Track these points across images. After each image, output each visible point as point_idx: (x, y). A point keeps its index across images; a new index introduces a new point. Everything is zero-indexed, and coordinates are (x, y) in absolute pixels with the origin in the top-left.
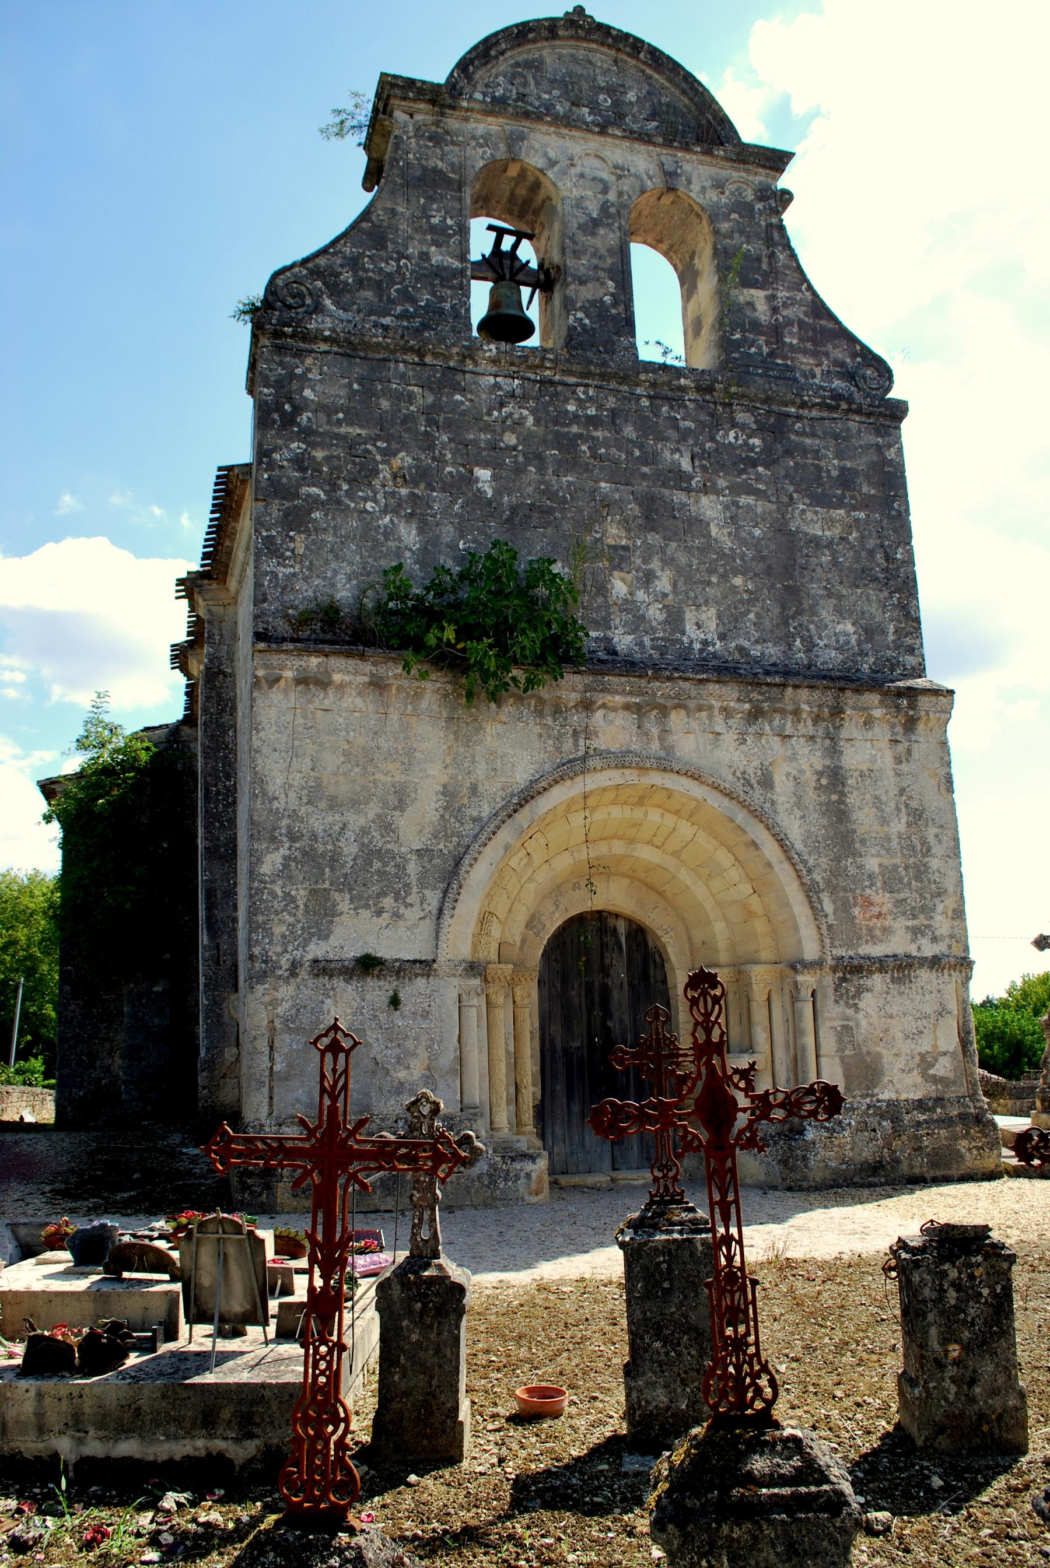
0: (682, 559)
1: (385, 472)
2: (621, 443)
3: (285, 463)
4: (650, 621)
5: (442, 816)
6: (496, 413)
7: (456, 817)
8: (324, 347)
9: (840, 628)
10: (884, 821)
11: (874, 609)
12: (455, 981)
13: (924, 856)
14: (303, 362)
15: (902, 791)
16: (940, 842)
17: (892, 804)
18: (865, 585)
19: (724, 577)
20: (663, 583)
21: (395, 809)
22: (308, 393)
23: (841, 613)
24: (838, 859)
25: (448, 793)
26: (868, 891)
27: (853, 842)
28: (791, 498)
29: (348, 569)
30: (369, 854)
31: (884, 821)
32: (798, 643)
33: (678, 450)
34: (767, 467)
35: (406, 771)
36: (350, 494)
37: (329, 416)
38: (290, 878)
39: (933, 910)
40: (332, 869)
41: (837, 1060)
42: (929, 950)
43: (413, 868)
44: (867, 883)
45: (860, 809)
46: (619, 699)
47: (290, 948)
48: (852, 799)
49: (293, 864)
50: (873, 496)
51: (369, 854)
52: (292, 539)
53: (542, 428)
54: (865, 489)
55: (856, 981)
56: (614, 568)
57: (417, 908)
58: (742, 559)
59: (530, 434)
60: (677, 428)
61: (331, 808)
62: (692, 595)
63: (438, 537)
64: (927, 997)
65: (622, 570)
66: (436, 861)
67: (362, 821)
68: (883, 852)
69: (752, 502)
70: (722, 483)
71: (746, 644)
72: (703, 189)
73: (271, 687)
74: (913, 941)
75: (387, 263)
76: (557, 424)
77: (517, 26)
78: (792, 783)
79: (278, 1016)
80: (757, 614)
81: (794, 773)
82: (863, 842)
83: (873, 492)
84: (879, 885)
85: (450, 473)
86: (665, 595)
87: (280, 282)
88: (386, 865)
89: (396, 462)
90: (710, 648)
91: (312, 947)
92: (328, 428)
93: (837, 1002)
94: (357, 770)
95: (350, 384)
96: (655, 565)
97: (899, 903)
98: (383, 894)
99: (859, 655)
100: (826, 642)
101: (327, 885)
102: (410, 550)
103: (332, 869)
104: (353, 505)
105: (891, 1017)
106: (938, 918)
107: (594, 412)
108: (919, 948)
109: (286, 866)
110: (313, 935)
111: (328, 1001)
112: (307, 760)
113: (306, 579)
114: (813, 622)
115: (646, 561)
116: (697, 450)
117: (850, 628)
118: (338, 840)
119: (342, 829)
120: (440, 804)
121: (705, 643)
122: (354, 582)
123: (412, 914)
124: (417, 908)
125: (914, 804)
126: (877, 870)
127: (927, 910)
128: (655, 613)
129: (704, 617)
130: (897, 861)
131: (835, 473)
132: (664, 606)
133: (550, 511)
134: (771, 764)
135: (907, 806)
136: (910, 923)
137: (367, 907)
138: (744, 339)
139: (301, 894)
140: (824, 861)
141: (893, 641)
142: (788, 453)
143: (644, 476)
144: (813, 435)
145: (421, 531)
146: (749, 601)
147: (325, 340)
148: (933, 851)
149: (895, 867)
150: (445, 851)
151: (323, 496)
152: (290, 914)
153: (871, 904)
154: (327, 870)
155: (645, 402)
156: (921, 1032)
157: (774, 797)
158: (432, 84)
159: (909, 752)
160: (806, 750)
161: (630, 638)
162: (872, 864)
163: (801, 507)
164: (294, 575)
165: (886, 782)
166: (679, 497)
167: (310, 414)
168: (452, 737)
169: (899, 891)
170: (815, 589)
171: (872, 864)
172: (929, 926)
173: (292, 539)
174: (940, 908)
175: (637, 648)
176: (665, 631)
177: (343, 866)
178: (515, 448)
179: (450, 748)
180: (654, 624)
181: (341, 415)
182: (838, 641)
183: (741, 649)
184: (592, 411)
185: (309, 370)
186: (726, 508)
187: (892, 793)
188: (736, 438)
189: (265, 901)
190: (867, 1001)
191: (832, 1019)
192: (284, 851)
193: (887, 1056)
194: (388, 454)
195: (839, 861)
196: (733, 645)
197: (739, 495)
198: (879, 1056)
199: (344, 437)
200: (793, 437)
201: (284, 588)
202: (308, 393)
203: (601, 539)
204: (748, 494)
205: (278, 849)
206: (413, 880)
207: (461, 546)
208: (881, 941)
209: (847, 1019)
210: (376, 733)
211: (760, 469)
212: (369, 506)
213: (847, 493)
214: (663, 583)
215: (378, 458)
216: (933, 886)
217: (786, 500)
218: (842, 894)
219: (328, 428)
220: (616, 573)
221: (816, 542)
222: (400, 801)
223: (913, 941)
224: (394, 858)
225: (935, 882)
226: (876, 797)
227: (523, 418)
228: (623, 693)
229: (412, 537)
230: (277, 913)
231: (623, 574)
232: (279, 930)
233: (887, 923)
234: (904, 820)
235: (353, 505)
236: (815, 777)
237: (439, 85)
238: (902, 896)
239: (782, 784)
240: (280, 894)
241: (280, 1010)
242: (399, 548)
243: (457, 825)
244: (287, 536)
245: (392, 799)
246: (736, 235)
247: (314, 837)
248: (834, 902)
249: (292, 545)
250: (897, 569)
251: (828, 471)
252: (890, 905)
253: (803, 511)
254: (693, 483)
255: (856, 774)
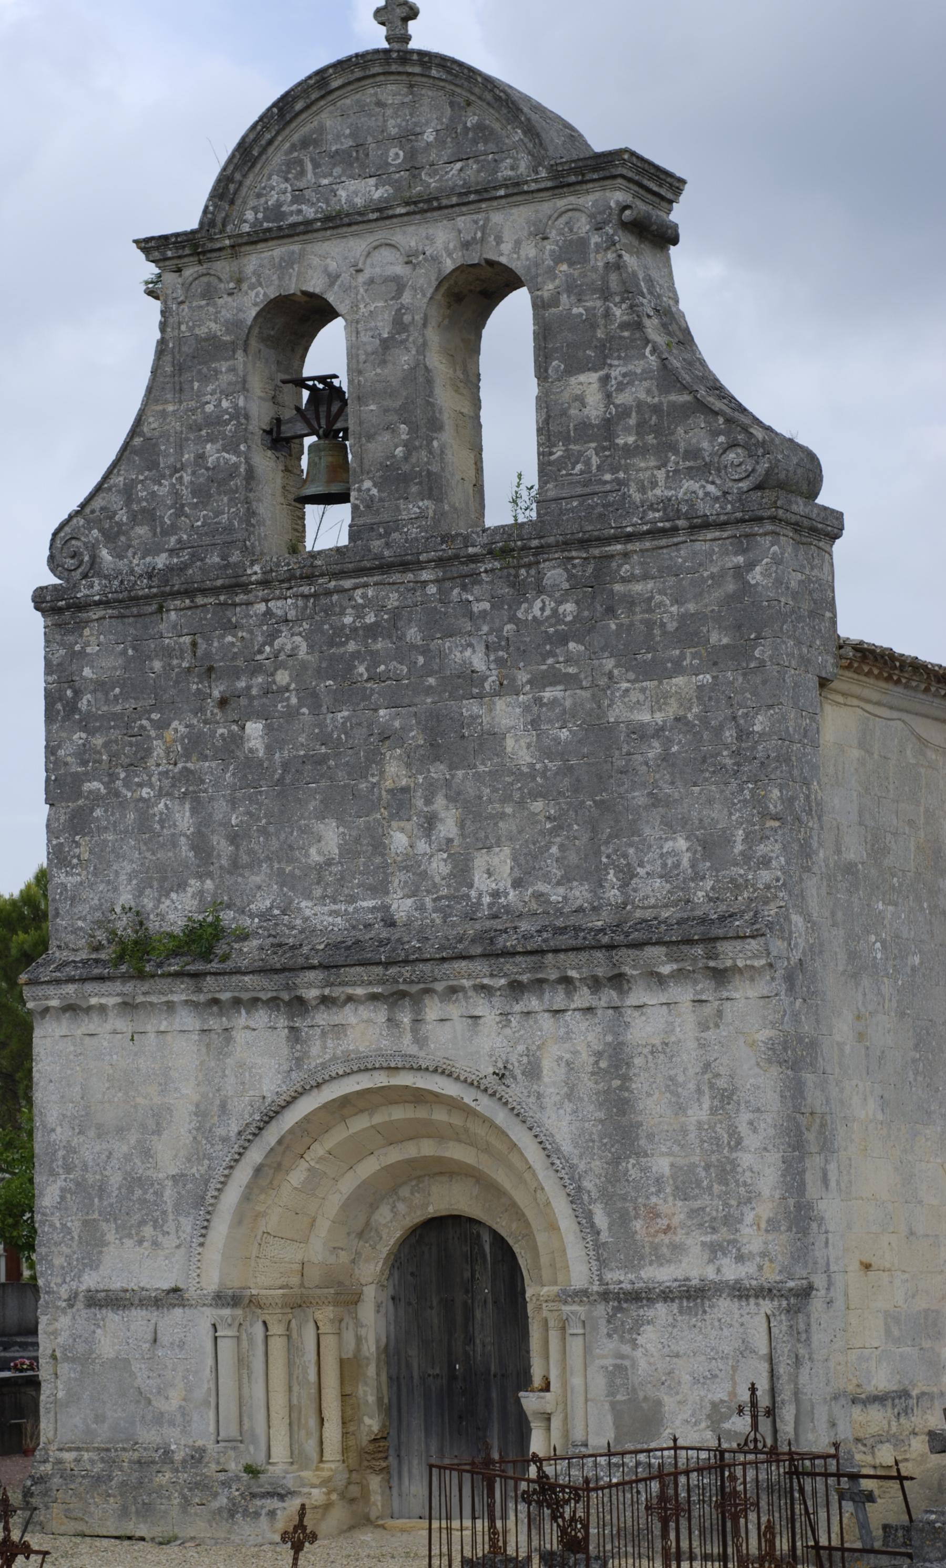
0: (470, 790)
1: (159, 748)
2: (403, 652)
3: (69, 759)
4: (432, 878)
5: (195, 1138)
6: (267, 649)
7: (207, 1138)
8: (100, 613)
9: (668, 846)
10: (680, 1108)
11: (717, 813)
12: (208, 1311)
13: (732, 1149)
14: (81, 636)
15: (707, 1066)
16: (755, 1130)
17: (692, 1086)
18: (706, 780)
19: (521, 803)
20: (448, 827)
21: (153, 1133)
22: (87, 672)
23: (670, 827)
24: (616, 1161)
25: (200, 1113)
26: (654, 1199)
27: (637, 1138)
28: (610, 675)
29: (129, 868)
30: (134, 1182)
31: (680, 1108)
32: (611, 876)
33: (470, 645)
34: (579, 641)
35: (163, 1092)
36: (127, 784)
37: (106, 694)
38: (66, 1209)
39: (740, 1221)
40: (101, 1199)
41: (607, 1406)
42: (732, 1271)
43: (169, 1194)
44: (653, 1189)
45: (649, 1095)
46: (360, 991)
47: (68, 1279)
48: (639, 1085)
49: (69, 1196)
50: (726, 647)
51: (134, 1182)
52: (78, 845)
53: (317, 655)
54: (714, 638)
55: (634, 1311)
56: (392, 817)
57: (173, 1236)
58: (544, 774)
59: (304, 665)
60: (471, 615)
61: (99, 1136)
62: (482, 834)
63: (211, 815)
64: (726, 1332)
65: (401, 819)
66: (190, 1186)
67: (125, 1149)
68: (676, 1149)
69: (559, 695)
70: (522, 677)
71: (542, 887)
72: (518, 243)
73: (43, 1018)
74: (711, 1261)
75: (160, 484)
76: (331, 644)
77: (275, 105)
78: (563, 1070)
79: (58, 1344)
80: (562, 847)
81: (567, 1056)
82: (650, 1137)
83: (725, 641)
84: (668, 1190)
85: (222, 735)
86: (449, 841)
87: (58, 543)
88: (145, 1192)
89: (169, 734)
90: (502, 900)
91: (86, 1277)
92: (105, 708)
93: (609, 1336)
94: (120, 1094)
95: (124, 652)
96: (440, 802)
97: (693, 1213)
98: (142, 1223)
99: (692, 880)
100: (648, 868)
101: (96, 1216)
102: (185, 835)
103: (101, 1199)
104: (129, 794)
105: (677, 1356)
106: (746, 1230)
107: (373, 620)
108: (719, 1270)
109: (63, 1198)
110: (85, 1265)
111: (99, 1331)
112: (78, 1088)
113: (91, 886)
114: (631, 845)
115: (428, 802)
116: (492, 638)
117: (682, 844)
118: (105, 1169)
119: (109, 1157)
120: (193, 1125)
121: (495, 894)
122: (134, 882)
123: (169, 1242)
124: (173, 1236)
125: (721, 1083)
126: (667, 1171)
127: (731, 1221)
128: (439, 867)
129: (496, 861)
130: (696, 1159)
131: (671, 626)
132: (450, 856)
133: (323, 759)
134: (539, 1048)
135: (712, 1086)
136: (708, 1239)
137: (130, 1236)
138: (568, 454)
139: (75, 1226)
140: (597, 1164)
141: (742, 853)
142: (610, 611)
143: (429, 690)
144: (645, 577)
145: (194, 811)
146: (551, 832)
147: (98, 604)
148: (746, 1143)
149: (692, 1167)
150: (197, 1176)
151: (103, 791)
152: (66, 1245)
153: (658, 1215)
154: (96, 1200)
155: (432, 589)
156: (716, 1376)
157: (542, 1088)
158: (185, 234)
159: (720, 1013)
160: (583, 1026)
161: (409, 902)
162: (662, 1165)
163: (625, 685)
164: (81, 883)
165: (685, 1057)
166: (471, 708)
167: (89, 696)
168: (204, 1050)
169: (695, 1198)
170: (639, 797)
171: (662, 1165)
172: (733, 1242)
173: (78, 845)
174: (749, 1217)
175: (417, 914)
176: (449, 886)
177: (109, 1196)
178: (287, 689)
179: (202, 1063)
180: (437, 879)
181: (117, 690)
182: (664, 865)
183: (538, 896)
184: (370, 619)
185: (87, 644)
186: (527, 709)
187: (691, 1072)
188: (542, 609)
189: (48, 1233)
190: (649, 1337)
191: (603, 1357)
192: (60, 1183)
193: (669, 1403)
194: (162, 726)
195: (618, 1164)
196: (530, 891)
197: (543, 688)
198: (659, 1403)
199: (115, 716)
200: (618, 587)
201: (73, 899)
202: (87, 672)
203: (378, 783)
204: (552, 684)
205: (54, 1181)
206: (169, 1207)
207: (233, 822)
208: (669, 1261)
209: (622, 1357)
210: (136, 1055)
211: (572, 645)
212: (145, 792)
213: (688, 652)
214: (448, 827)
215: (153, 733)
216: (742, 1190)
217: (603, 681)
218: (619, 1205)
219: (105, 708)
220: (394, 824)
221: (640, 733)
222: (158, 1124)
223: (711, 1261)
224: (152, 1185)
225: (745, 1184)
226: (671, 1079)
227: (296, 648)
228: (362, 983)
229: (186, 820)
230: (57, 1244)
231: (402, 824)
232: (58, 1261)
233: (677, 1239)
234: (706, 1106)
235: (129, 794)
236: (592, 1059)
237: (193, 232)
238: (697, 1204)
239: (552, 1073)
240: (58, 1225)
241: (60, 1340)
242: (173, 835)
243: (208, 1146)
244: (74, 841)
245: (151, 1123)
246: (564, 298)
247: (85, 1168)
248: (609, 1215)
249: (77, 851)
250: (753, 748)
251: (663, 625)
252: (682, 1216)
253: (627, 691)
254: (487, 686)
255: (646, 1051)
